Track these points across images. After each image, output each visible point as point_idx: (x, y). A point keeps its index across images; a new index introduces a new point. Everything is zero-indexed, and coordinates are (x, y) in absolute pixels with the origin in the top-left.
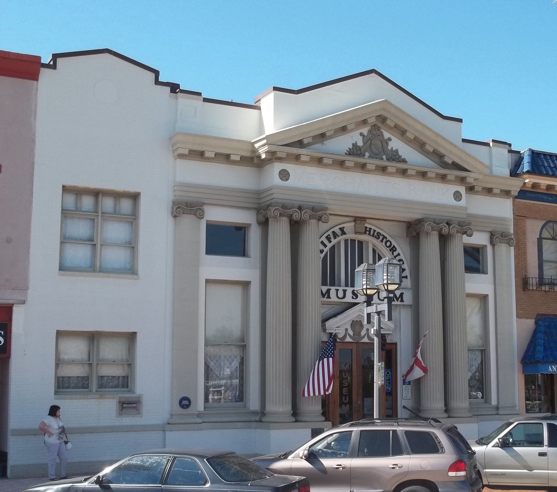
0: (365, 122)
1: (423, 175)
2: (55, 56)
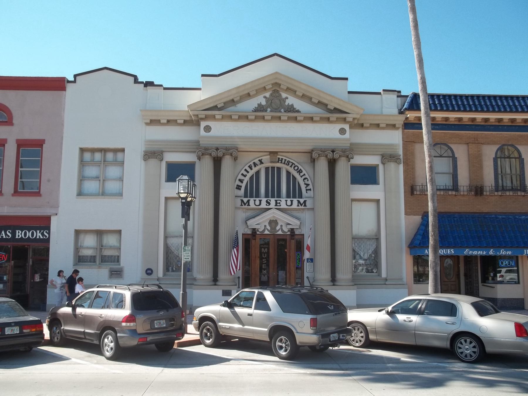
0: (265, 89)
1: (311, 119)
2: (75, 76)
